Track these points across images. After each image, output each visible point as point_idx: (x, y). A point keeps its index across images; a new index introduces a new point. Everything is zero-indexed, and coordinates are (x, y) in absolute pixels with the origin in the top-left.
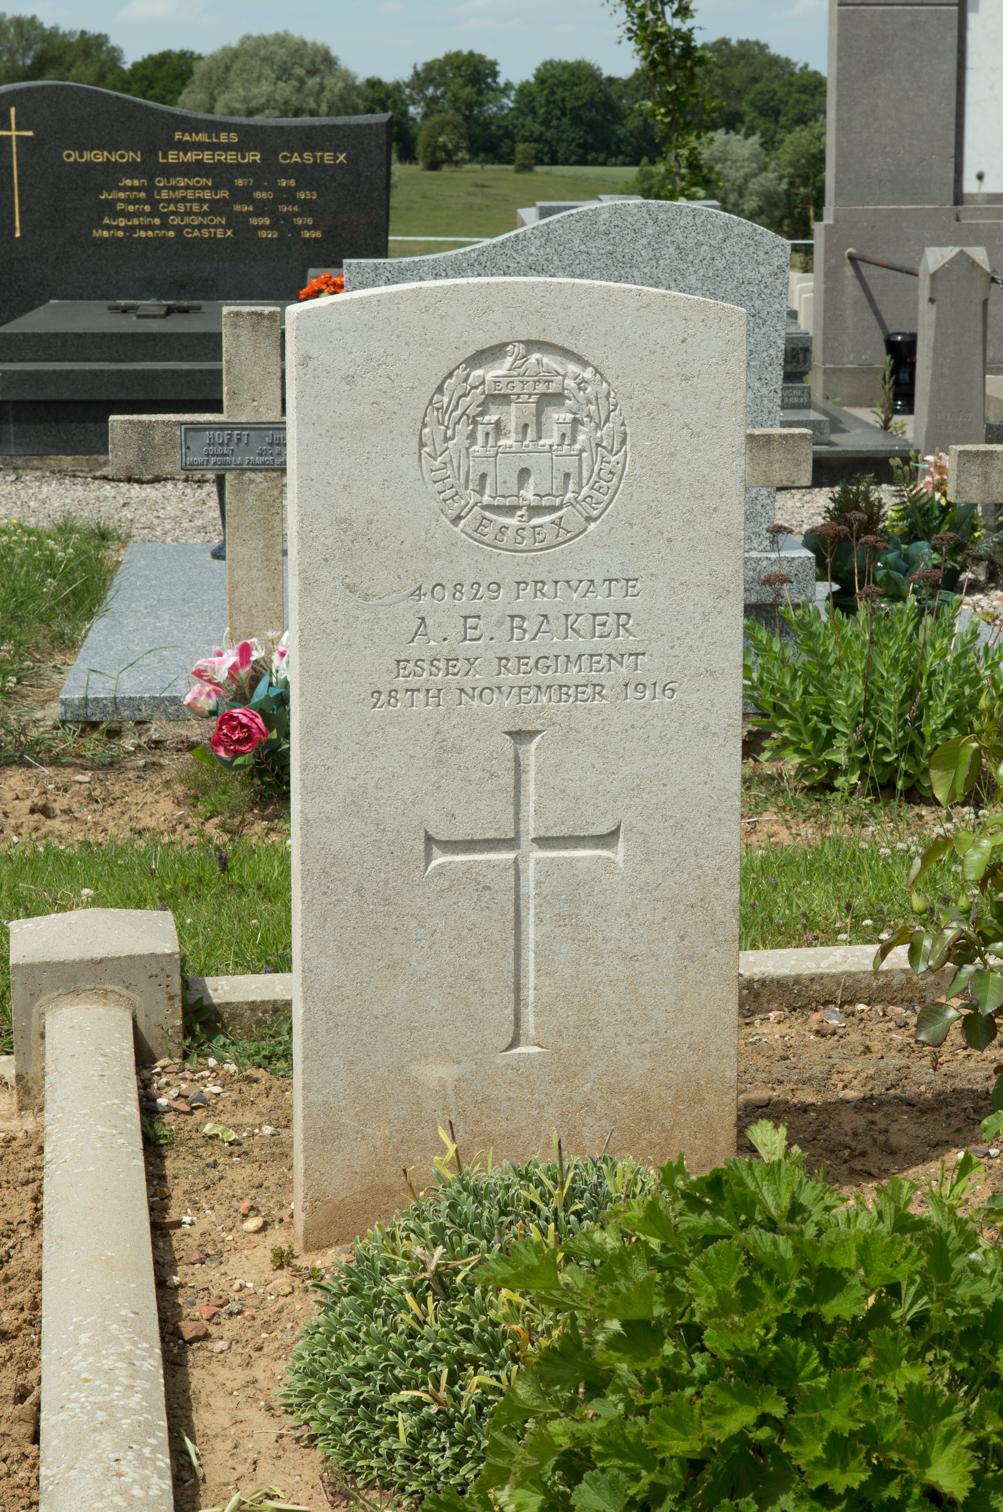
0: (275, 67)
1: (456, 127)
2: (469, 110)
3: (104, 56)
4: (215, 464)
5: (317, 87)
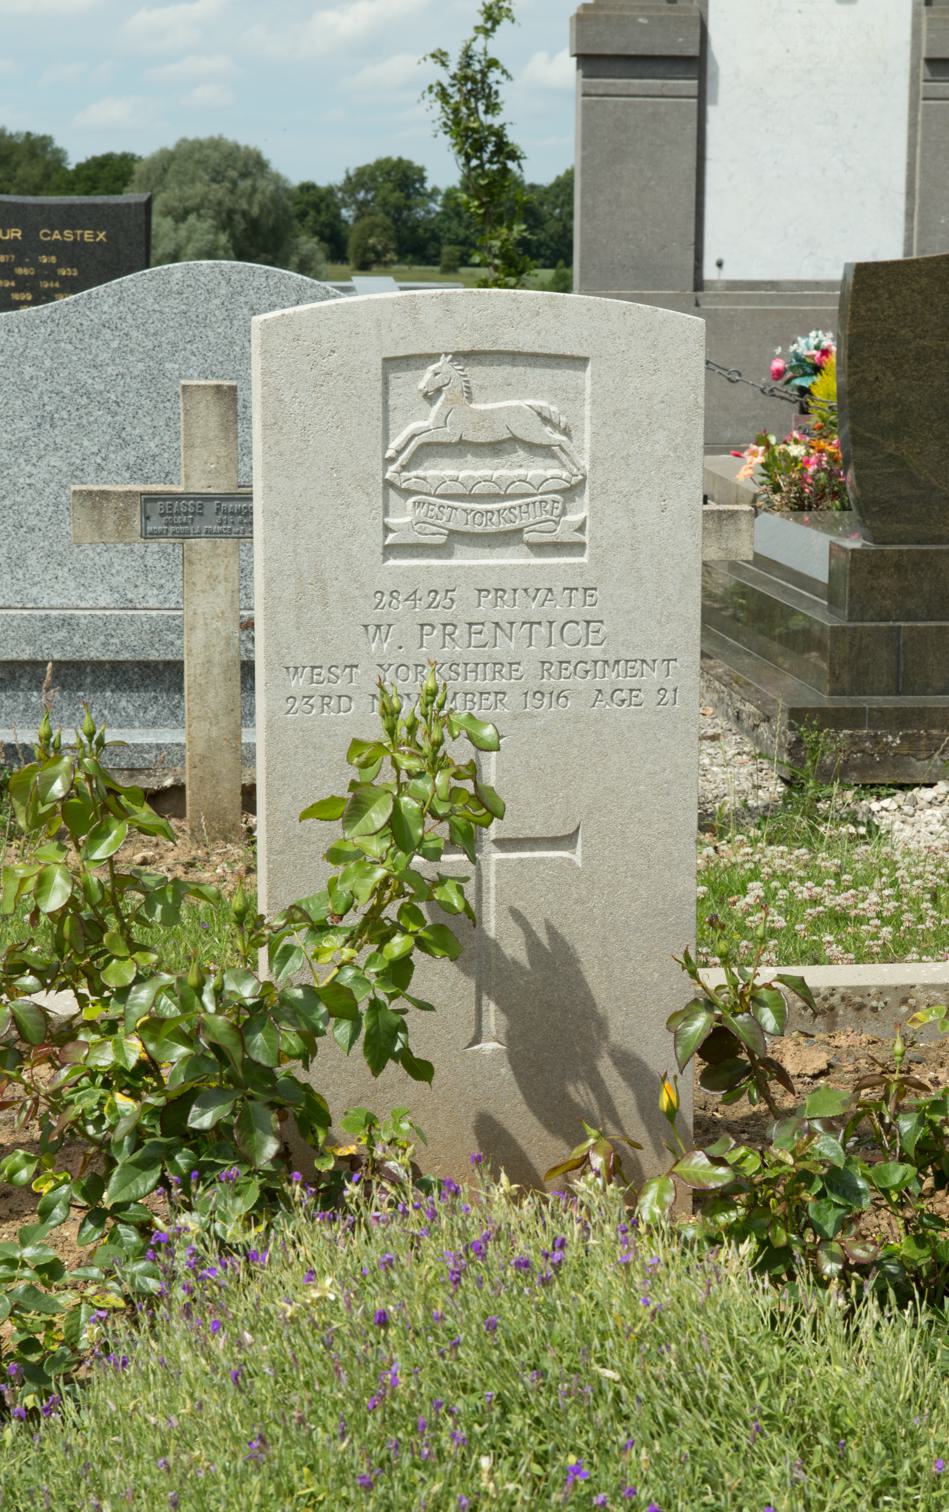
0: (210, 170)
1: (385, 229)
2: (398, 214)
3: (49, 157)
4: (174, 533)
5: (250, 189)
